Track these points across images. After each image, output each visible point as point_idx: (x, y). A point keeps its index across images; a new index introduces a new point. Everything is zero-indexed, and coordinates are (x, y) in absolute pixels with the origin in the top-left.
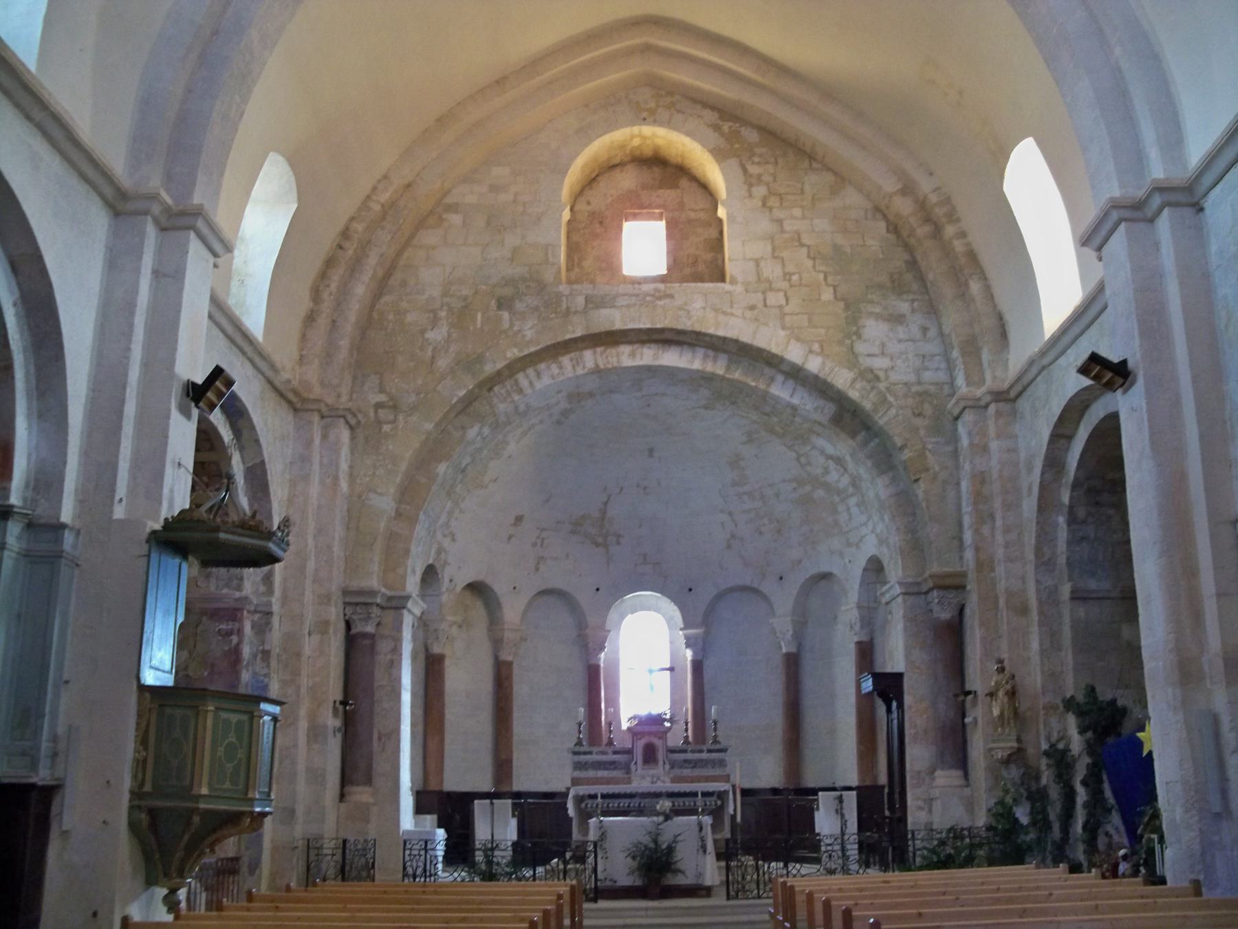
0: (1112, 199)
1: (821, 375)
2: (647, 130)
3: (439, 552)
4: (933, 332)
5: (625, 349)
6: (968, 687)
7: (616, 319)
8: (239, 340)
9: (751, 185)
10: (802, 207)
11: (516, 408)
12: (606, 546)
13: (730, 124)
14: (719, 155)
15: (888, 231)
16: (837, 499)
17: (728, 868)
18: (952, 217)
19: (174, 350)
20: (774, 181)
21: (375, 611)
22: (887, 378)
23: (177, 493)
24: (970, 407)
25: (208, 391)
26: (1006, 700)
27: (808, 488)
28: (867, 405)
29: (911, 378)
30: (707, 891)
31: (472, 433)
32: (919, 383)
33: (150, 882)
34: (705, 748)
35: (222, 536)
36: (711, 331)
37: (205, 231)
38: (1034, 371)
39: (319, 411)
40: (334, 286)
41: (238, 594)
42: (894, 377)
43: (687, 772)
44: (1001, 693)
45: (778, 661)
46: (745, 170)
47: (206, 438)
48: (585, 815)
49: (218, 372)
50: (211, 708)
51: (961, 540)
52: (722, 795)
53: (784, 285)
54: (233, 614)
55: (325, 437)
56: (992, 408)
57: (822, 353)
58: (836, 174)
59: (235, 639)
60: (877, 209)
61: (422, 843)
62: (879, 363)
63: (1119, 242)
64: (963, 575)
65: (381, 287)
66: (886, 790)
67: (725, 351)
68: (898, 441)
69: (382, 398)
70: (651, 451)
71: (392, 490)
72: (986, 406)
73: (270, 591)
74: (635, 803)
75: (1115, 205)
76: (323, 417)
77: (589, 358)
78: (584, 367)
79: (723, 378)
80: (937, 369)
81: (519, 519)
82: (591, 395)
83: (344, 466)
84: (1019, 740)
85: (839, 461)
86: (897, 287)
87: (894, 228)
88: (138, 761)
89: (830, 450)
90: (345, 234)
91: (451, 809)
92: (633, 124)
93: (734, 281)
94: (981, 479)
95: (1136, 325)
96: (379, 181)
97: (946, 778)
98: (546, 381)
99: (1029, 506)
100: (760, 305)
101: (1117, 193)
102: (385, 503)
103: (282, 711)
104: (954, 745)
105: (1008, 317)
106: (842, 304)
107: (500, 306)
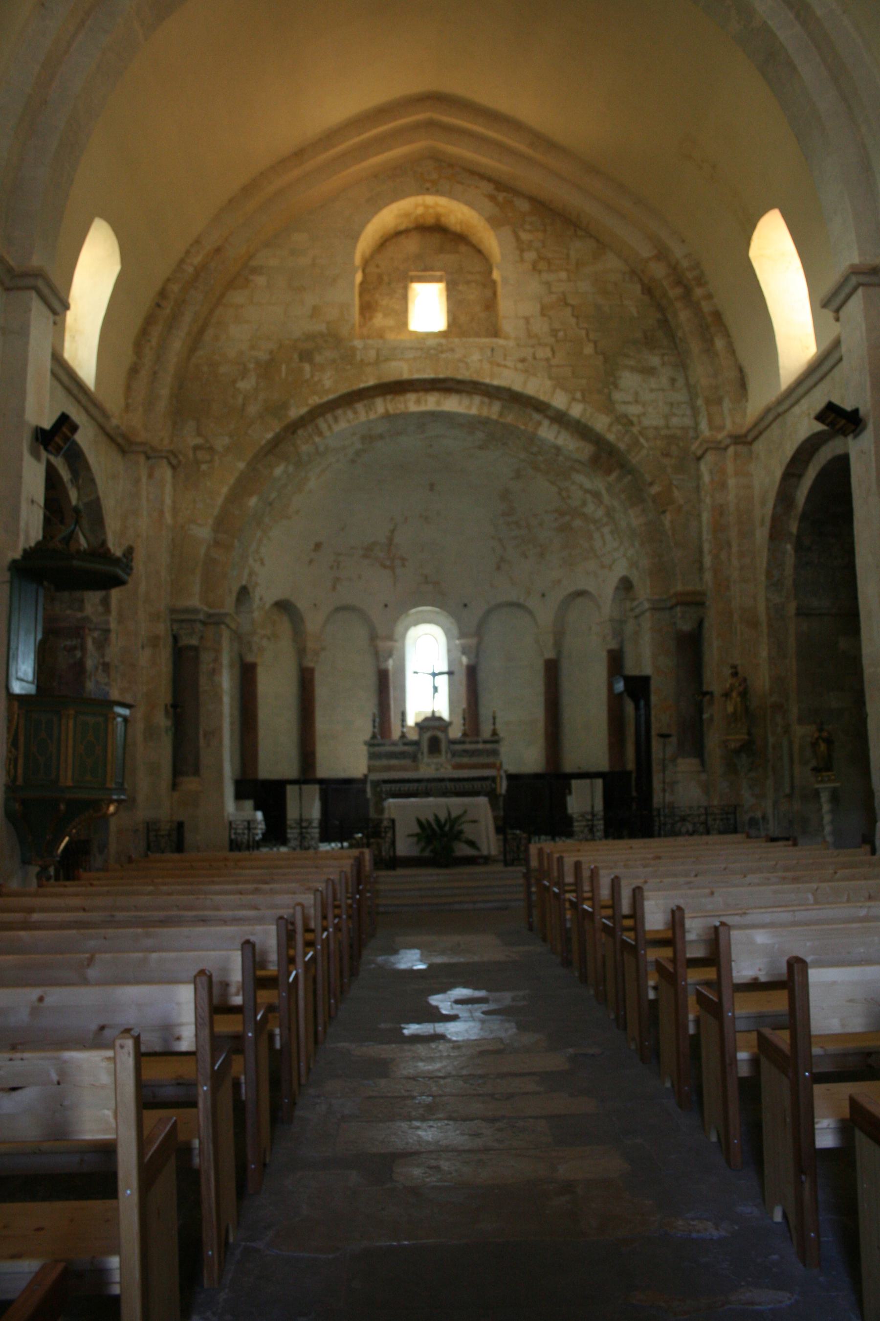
0: (852, 266)
1: (583, 420)
2: (430, 200)
3: (251, 574)
4: (680, 382)
5: (412, 397)
6: (705, 688)
7: (403, 370)
8: (75, 391)
9: (522, 251)
10: (567, 270)
11: (317, 449)
12: (392, 568)
13: (505, 194)
14: (495, 222)
15: (643, 293)
16: (592, 527)
17: (505, 841)
18: (700, 281)
19: (23, 399)
20: (544, 247)
21: (199, 627)
22: (640, 422)
23: (31, 526)
24: (711, 448)
25: (56, 438)
26: (739, 699)
27: (567, 518)
28: (622, 446)
29: (661, 423)
30: (487, 860)
31: (278, 471)
32: (668, 427)
33: (25, 862)
34: (480, 739)
35: (76, 563)
36: (487, 381)
37: (46, 291)
38: (770, 417)
39: (145, 453)
40: (154, 341)
41: (79, 615)
42: (646, 422)
43: (465, 760)
44: (734, 694)
45: (539, 666)
46: (518, 238)
47: (52, 479)
48: (380, 798)
49: (64, 419)
50: (72, 712)
51: (700, 562)
52: (493, 779)
53: (552, 340)
54: (78, 631)
55: (150, 476)
56: (731, 450)
57: (583, 400)
58: (597, 240)
59: (78, 654)
60: (633, 272)
61: (246, 823)
62: (633, 410)
63: (855, 306)
64: (703, 594)
65: (195, 342)
66: (634, 776)
67: (499, 399)
68: (648, 478)
69: (199, 441)
70: (432, 487)
71: (211, 521)
72: (726, 449)
73: (108, 610)
74: (422, 786)
75: (855, 271)
76: (148, 458)
77: (381, 406)
78: (376, 413)
79: (496, 422)
80: (683, 415)
81: (318, 546)
82: (381, 437)
83: (168, 501)
84: (749, 734)
85: (596, 495)
86: (649, 342)
87: (648, 290)
88: (10, 760)
89: (588, 485)
90: (163, 294)
91: (266, 794)
92: (418, 193)
93: (506, 338)
94: (720, 511)
95: (868, 378)
96: (192, 245)
97: (686, 765)
98: (343, 425)
99: (761, 535)
100: (530, 358)
101: (856, 260)
102: (203, 532)
103: (131, 713)
104: (692, 737)
105: (748, 370)
106: (601, 358)
107: (301, 359)
